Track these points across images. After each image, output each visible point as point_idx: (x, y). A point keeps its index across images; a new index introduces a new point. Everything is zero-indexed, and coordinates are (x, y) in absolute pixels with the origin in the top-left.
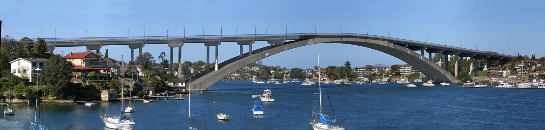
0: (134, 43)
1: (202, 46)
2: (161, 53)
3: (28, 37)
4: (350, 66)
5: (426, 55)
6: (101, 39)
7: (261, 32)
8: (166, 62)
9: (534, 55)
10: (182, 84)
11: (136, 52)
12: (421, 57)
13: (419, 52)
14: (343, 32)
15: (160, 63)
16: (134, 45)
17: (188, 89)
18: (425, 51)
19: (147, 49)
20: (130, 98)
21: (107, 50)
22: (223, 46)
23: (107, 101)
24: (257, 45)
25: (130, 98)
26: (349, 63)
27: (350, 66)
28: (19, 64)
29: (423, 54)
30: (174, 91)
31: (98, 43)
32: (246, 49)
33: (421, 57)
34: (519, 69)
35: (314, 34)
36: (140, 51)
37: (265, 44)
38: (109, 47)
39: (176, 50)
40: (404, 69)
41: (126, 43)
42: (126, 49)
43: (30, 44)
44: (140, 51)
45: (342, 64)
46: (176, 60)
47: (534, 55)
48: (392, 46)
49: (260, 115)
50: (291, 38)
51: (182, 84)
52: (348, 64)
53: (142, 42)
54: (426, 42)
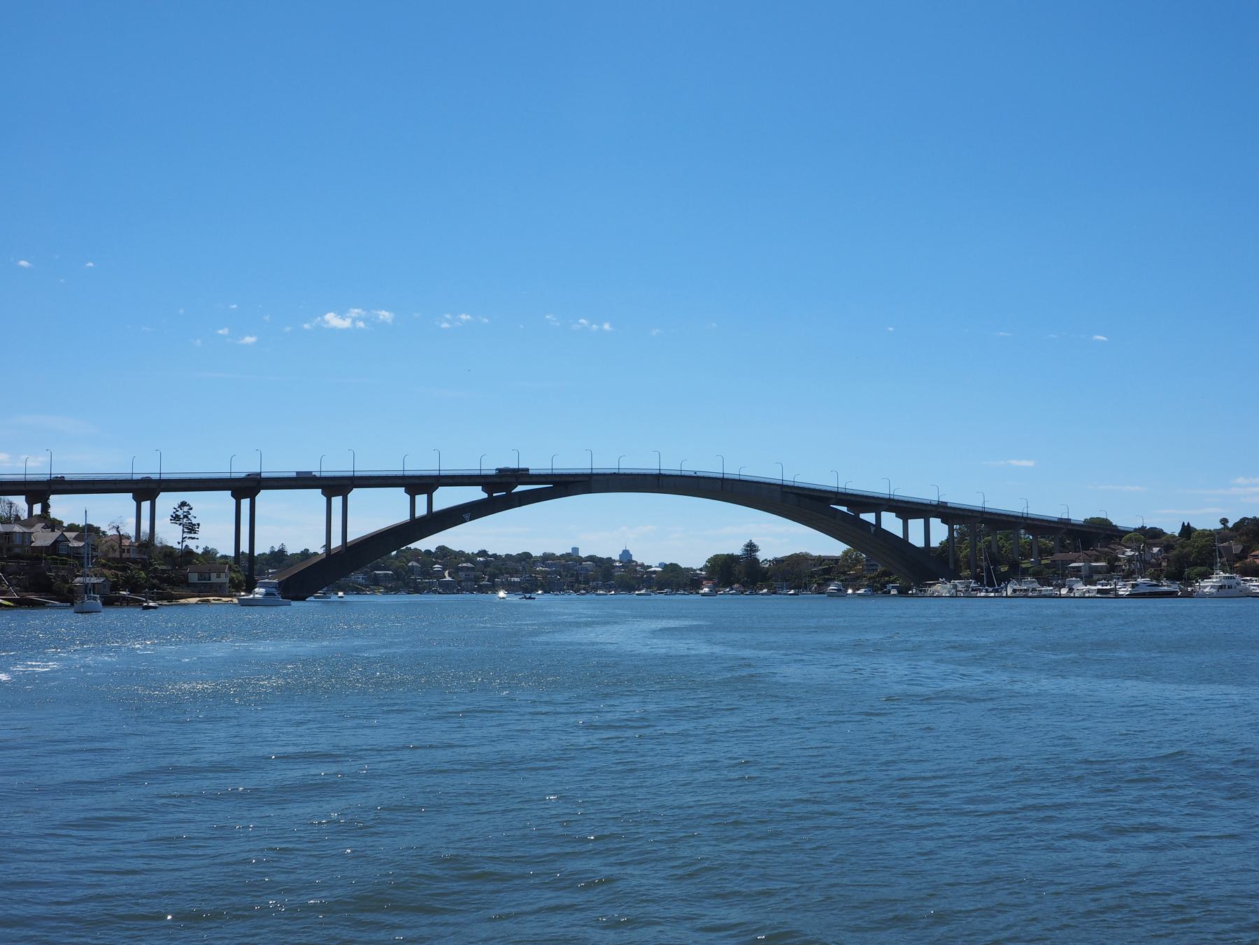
1: (400, 494)
11: (421, 500)
13: (869, 517)
24: (446, 498)
26: (754, 546)
29: (878, 519)
52: (575, 550)
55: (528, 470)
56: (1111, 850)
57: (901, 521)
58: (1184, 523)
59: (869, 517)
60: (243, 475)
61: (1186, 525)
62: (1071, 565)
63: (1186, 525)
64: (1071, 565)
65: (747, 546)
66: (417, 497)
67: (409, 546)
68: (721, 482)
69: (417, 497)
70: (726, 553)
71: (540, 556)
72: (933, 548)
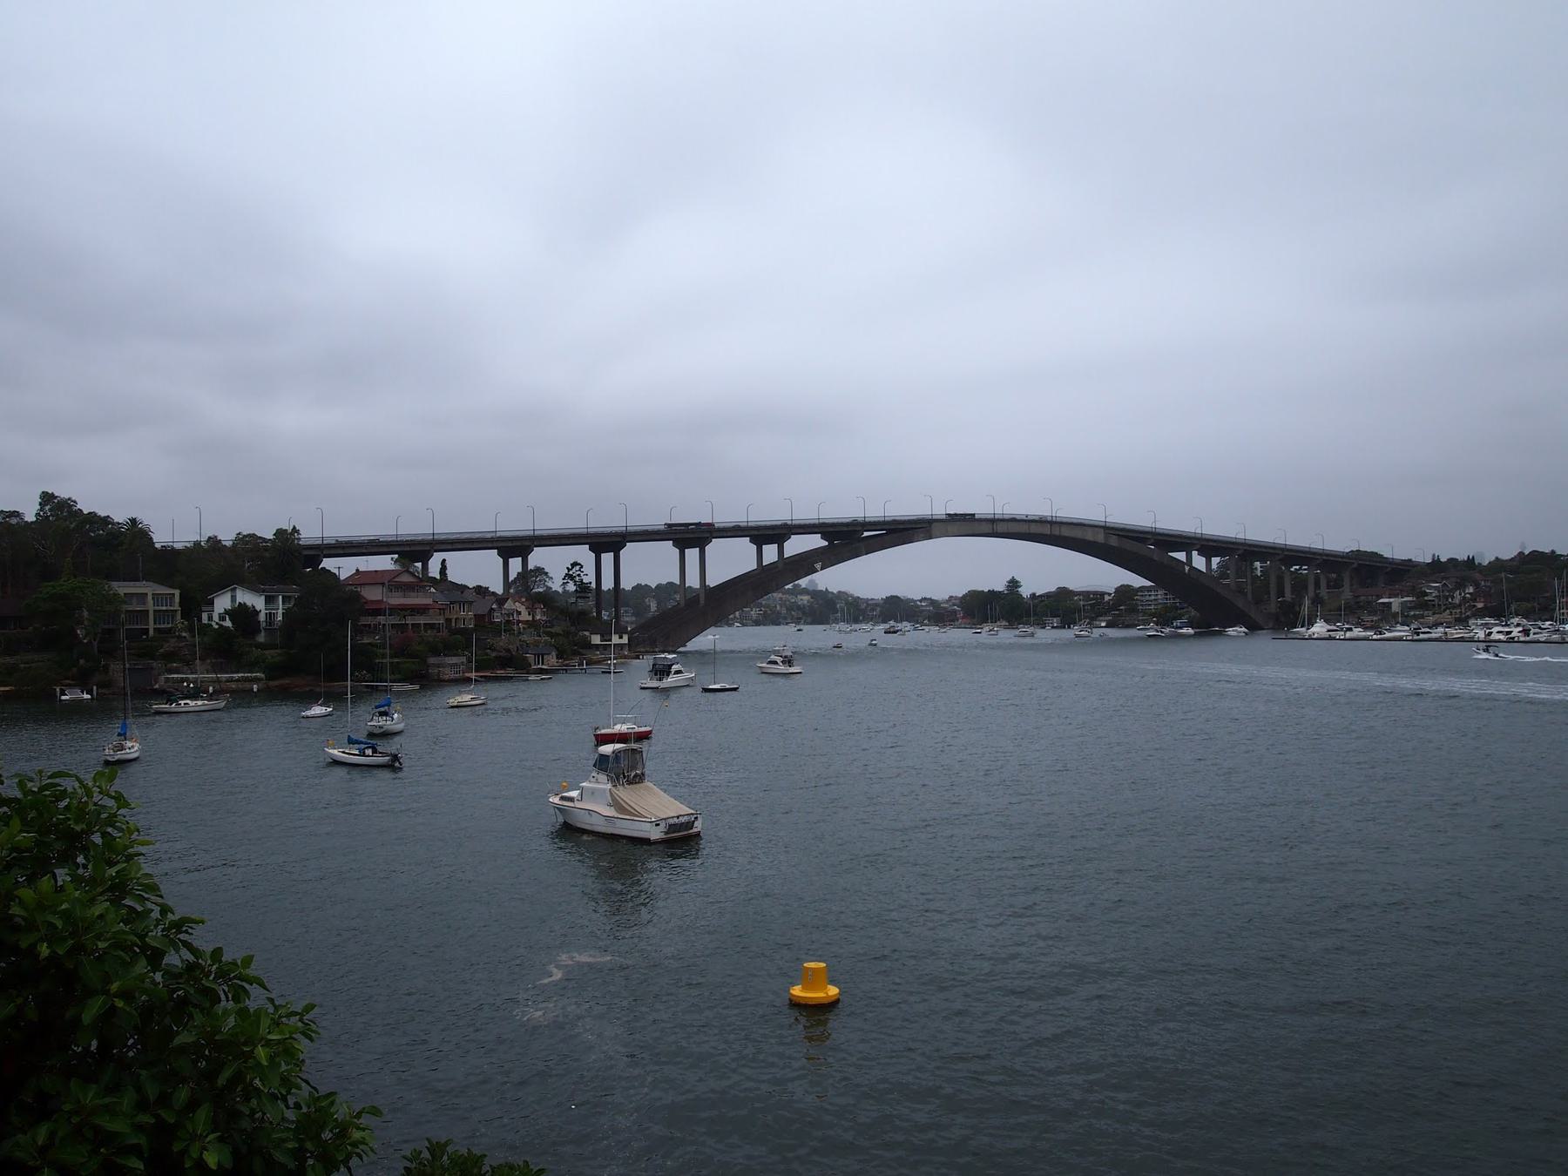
0: (405, 549)
1: (668, 549)
2: (568, 568)
3: (958, 512)
4: (78, 507)
5: (1199, 562)
6: (625, 529)
7: (805, 513)
8: (583, 588)
9: (1473, 557)
10: (621, 637)
11: (516, 565)
12: (1187, 568)
13: (1181, 556)
14: (998, 511)
15: (961, 596)
16: (513, 547)
17: (287, 606)
18: (1195, 553)
19: (538, 557)
20: (474, 674)
21: (444, 561)
22: (715, 547)
23: (656, 842)
24: (797, 545)
25: (474, 674)
26: (1017, 582)
27: (1020, 589)
28: (233, 598)
29: (1189, 557)
30: (1335, 625)
31: (619, 539)
32: (770, 553)
33: (1187, 568)
34: (1434, 595)
35: (817, 522)
36: (781, 551)
37: (816, 542)
38: (451, 557)
39: (608, 558)
40: (1147, 598)
41: (816, 530)
42: (492, 557)
43: (248, 544)
44: (781, 551)
45: (1000, 586)
46: (608, 583)
47: (1473, 557)
48: (1114, 541)
49: (156, 704)
50: (874, 528)
51: (621, 637)
52: (1014, 584)
53: (527, 543)
54: (1199, 531)
55: (974, 515)
56: (759, 1089)
57: (1204, 559)
58: (1434, 555)
59: (1181, 556)
60: (780, 523)
61: (1471, 557)
62: (1380, 601)
63: (1471, 557)
64: (1380, 601)
65: (1009, 582)
66: (511, 560)
67: (796, 582)
68: (1049, 526)
69: (511, 560)
70: (980, 589)
71: (832, 593)
72: (344, 580)
